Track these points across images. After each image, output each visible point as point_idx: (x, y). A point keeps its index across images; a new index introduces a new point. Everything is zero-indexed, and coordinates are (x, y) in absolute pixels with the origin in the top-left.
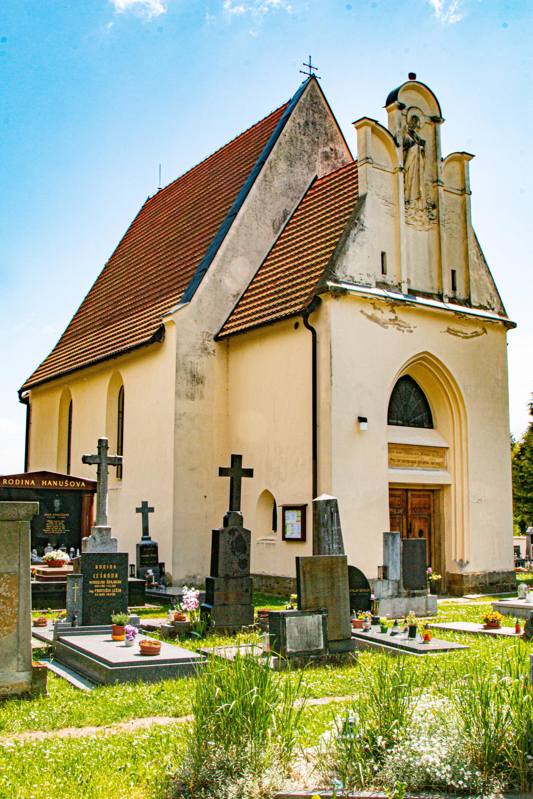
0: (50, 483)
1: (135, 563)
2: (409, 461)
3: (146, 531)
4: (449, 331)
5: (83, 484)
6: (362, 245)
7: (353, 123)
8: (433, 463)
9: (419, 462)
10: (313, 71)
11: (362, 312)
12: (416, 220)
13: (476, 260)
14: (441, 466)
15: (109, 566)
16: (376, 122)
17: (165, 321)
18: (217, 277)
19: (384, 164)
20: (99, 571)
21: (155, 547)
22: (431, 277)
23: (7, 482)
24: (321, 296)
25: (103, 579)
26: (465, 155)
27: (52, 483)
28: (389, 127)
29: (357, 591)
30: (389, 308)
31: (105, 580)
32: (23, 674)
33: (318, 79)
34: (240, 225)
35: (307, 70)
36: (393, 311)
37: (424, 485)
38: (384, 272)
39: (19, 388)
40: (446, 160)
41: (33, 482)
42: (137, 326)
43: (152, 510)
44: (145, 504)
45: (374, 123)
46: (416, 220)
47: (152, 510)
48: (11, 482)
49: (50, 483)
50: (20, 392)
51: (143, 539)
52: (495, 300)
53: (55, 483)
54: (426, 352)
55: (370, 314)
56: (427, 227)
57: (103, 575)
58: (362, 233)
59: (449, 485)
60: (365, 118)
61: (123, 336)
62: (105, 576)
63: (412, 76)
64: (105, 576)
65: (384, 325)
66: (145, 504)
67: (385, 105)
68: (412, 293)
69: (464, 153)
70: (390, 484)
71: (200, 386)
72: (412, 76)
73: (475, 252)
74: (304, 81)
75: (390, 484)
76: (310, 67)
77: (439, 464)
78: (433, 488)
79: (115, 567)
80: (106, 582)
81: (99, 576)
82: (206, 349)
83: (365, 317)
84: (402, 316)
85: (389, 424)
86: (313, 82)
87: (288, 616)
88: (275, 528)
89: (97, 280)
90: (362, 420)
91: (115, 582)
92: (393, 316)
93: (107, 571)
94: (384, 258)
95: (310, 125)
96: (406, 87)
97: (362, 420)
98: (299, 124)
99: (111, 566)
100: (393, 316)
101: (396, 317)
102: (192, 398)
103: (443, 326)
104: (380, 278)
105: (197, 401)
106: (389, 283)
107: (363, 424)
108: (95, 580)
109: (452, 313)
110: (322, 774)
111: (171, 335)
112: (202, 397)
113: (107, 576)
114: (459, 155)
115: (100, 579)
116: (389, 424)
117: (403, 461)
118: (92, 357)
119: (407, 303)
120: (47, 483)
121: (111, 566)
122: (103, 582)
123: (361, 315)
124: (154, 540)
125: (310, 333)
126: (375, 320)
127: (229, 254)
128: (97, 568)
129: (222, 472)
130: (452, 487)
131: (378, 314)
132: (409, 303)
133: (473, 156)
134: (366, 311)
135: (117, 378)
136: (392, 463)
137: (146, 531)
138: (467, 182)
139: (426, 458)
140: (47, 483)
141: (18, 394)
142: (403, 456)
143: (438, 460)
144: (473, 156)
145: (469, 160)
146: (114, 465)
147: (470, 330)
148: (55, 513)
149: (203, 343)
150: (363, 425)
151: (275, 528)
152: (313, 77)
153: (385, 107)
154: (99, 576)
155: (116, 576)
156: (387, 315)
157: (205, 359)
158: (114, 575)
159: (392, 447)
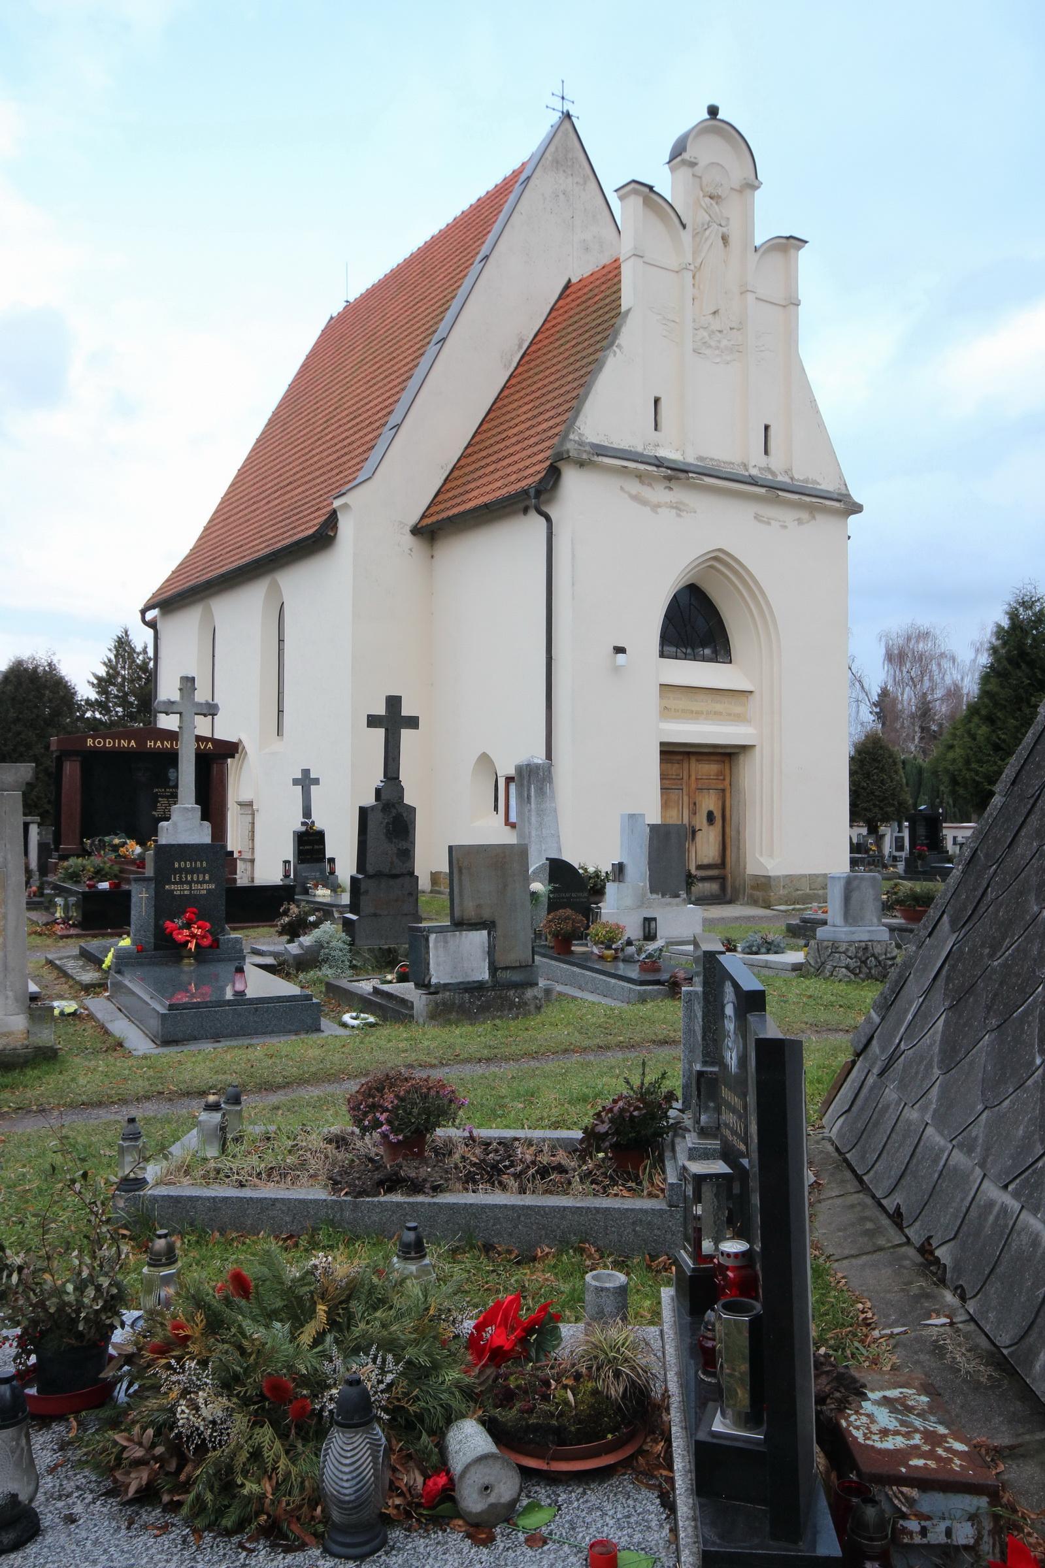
0: (159, 744)
1: (291, 858)
2: (692, 712)
3: (307, 813)
5: (210, 745)
7: (616, 191)
8: (730, 715)
9: (708, 713)
10: (568, 107)
12: (710, 347)
14: (740, 718)
15: (196, 863)
16: (651, 188)
17: (337, 504)
20: (180, 871)
21: (320, 836)
23: (94, 743)
24: (559, 464)
25: (187, 882)
26: (792, 241)
27: (163, 744)
28: (673, 196)
29: (568, 895)
31: (190, 883)
32: (18, 1017)
33: (573, 119)
35: (558, 104)
39: (141, 606)
40: (762, 250)
41: (133, 743)
42: (302, 511)
43: (316, 781)
44: (306, 772)
45: (647, 190)
46: (710, 347)
47: (316, 781)
48: (99, 743)
49: (159, 744)
50: (143, 612)
51: (303, 824)
53: (124, 743)
54: (720, 550)
55: (634, 492)
57: (186, 877)
59: (753, 746)
60: (634, 181)
61: (282, 527)
62: (189, 878)
63: (713, 111)
64: (189, 878)
66: (306, 772)
67: (668, 160)
70: (662, 744)
72: (713, 111)
74: (552, 123)
75: (662, 744)
78: (728, 751)
79: (204, 864)
80: (191, 887)
81: (181, 878)
83: (626, 496)
85: (662, 655)
86: (567, 124)
87: (432, 932)
88: (496, 808)
89: (256, 443)
90: (620, 650)
91: (205, 886)
93: (192, 871)
94: (659, 408)
95: (562, 196)
96: (701, 130)
97: (620, 650)
98: (543, 195)
99: (198, 863)
107: (620, 656)
108: (174, 883)
111: (346, 527)
113: (192, 878)
114: (784, 241)
115: (181, 883)
116: (662, 655)
117: (683, 711)
118: (239, 559)
119: (691, 475)
120: (155, 744)
121: (198, 863)
122: (186, 887)
124: (318, 826)
125: (543, 520)
126: (644, 502)
128: (176, 865)
130: (757, 748)
132: (694, 475)
133: (806, 242)
135: (275, 590)
136: (666, 713)
137: (307, 813)
139: (718, 707)
140: (155, 744)
141: (139, 616)
142: (683, 703)
143: (738, 709)
144: (806, 242)
145: (799, 248)
146: (205, 715)
148: (170, 788)
151: (496, 808)
152: (568, 116)
153: (669, 163)
154: (181, 878)
155: (207, 878)
158: (204, 877)
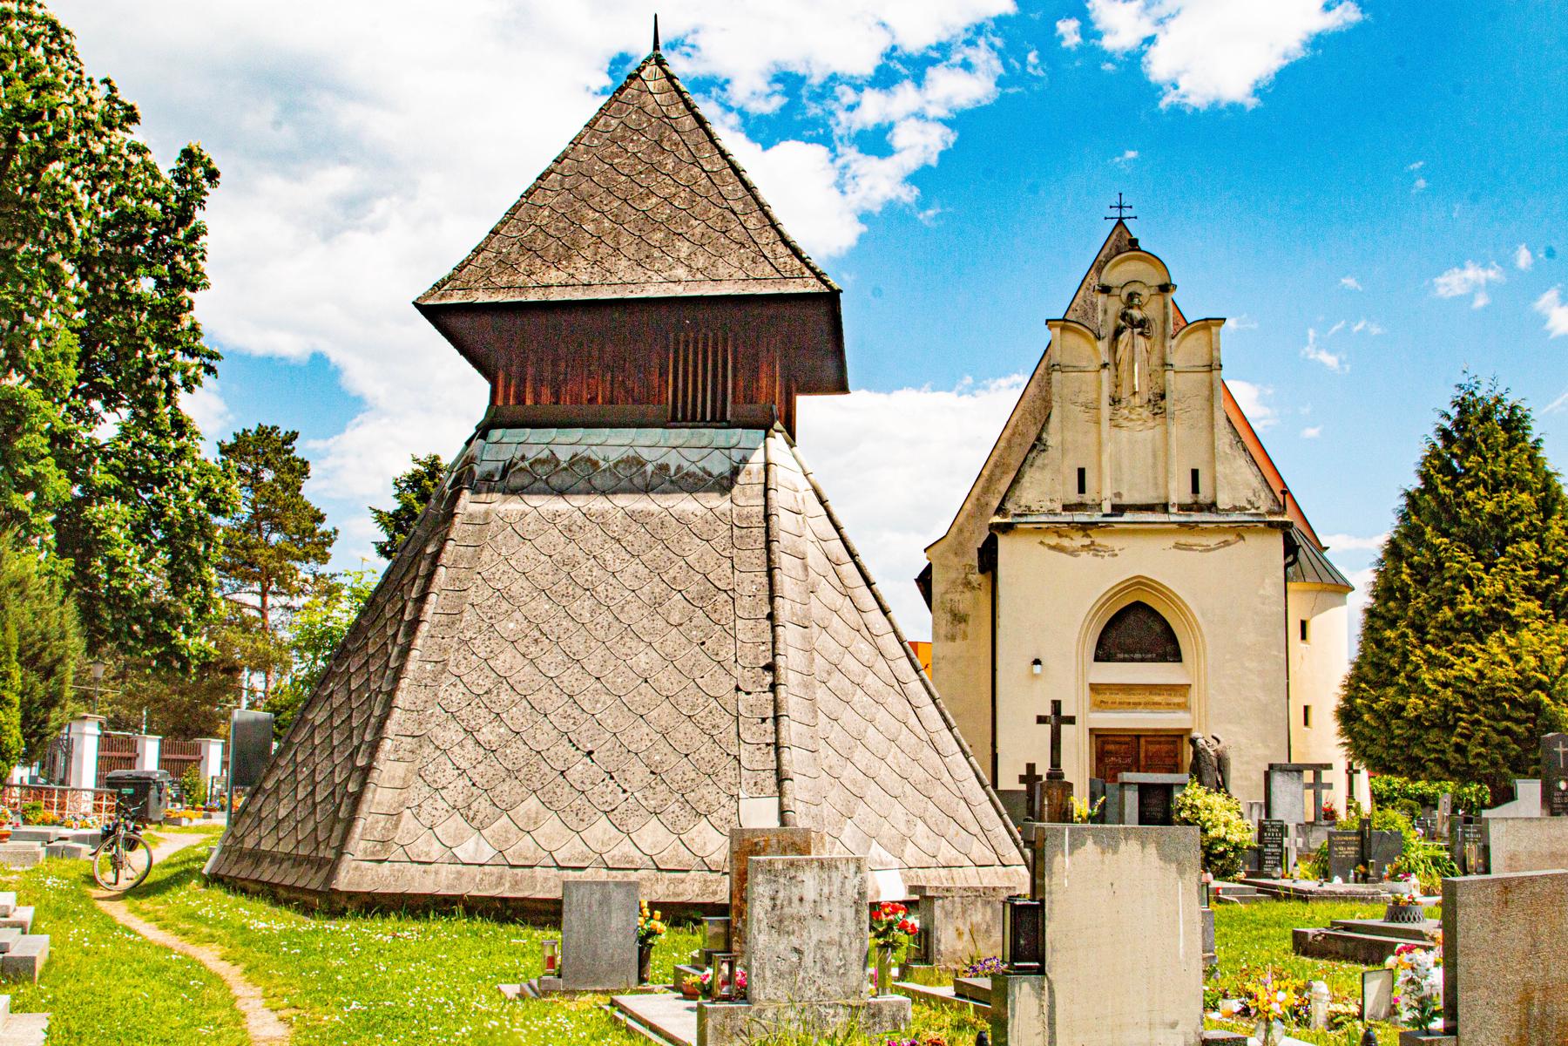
4: (1178, 546)
6: (1044, 467)
8: (1169, 704)
9: (1146, 704)
11: (1041, 543)
12: (1132, 420)
13: (1228, 450)
14: (1184, 707)
18: (982, 500)
19: (1084, 364)
22: (1156, 484)
30: (1081, 533)
34: (1013, 434)
36: (1088, 536)
37: (1156, 730)
38: (1082, 489)
46: (1132, 420)
52: (1263, 495)
56: (1152, 424)
58: (1043, 454)
65: (1073, 553)
68: (1118, 509)
69: (1206, 320)
71: (963, 625)
73: (1227, 441)
76: (1121, 207)
77: (1179, 705)
82: (969, 583)
84: (1100, 539)
92: (1087, 541)
97: (1037, 662)
100: (1087, 541)
101: (1093, 543)
102: (953, 638)
103: (1170, 541)
104: (1074, 497)
105: (958, 641)
106: (1090, 502)
109: (1175, 526)
110: (457, 790)
112: (965, 637)
123: (1041, 547)
127: (998, 472)
129: (1041, 720)
131: (1065, 542)
134: (1047, 541)
138: (1215, 354)
143: (1177, 700)
147: (1213, 541)
149: (966, 577)
150: (1037, 668)
156: (1079, 540)
157: (968, 595)
159: (1095, 688)
